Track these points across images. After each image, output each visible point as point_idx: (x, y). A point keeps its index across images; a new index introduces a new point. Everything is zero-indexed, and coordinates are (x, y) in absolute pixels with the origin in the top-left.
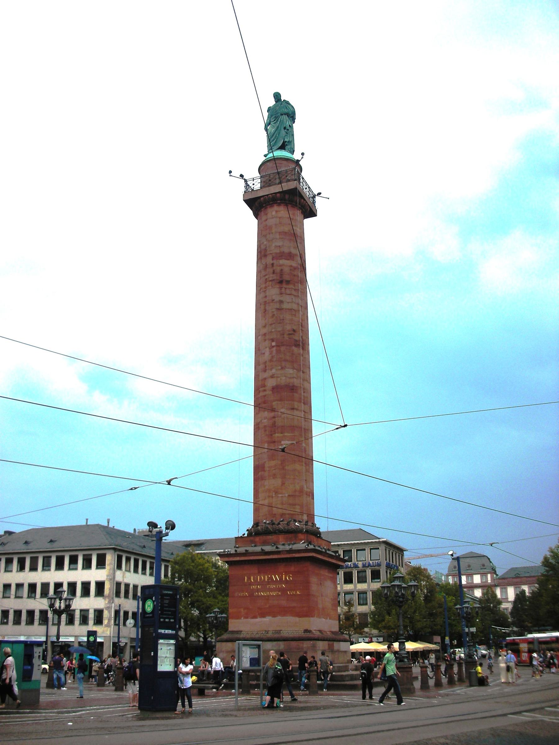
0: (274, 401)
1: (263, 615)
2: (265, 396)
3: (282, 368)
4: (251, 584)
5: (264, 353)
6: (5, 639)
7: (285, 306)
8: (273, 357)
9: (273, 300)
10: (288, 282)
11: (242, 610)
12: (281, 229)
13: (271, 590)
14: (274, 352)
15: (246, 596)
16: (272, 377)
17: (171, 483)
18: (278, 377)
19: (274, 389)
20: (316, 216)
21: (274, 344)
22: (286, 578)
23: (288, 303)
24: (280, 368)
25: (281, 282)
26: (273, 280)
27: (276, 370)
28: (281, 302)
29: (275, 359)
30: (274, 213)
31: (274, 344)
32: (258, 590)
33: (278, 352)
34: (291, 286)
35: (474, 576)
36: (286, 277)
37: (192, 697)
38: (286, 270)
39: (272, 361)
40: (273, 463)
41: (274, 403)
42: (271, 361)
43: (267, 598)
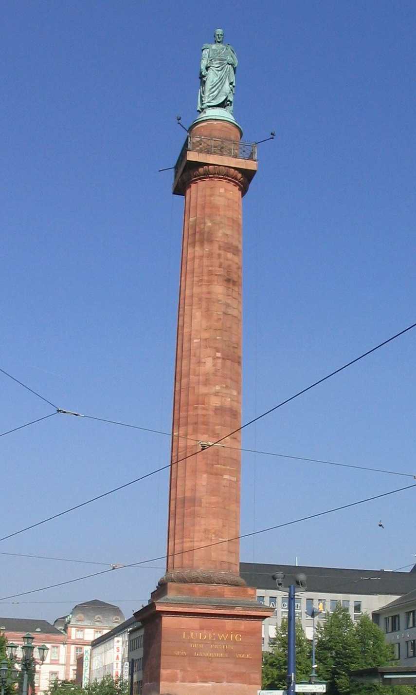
1: (205, 680)
3: (227, 387)
6: (264, 590)
7: (230, 311)
8: (216, 371)
9: (219, 301)
10: (234, 283)
11: (178, 671)
12: (230, 214)
14: (219, 366)
16: (216, 394)
19: (216, 410)
20: (174, 193)
21: (218, 355)
22: (234, 638)
23: (234, 308)
24: (224, 386)
25: (228, 280)
26: (220, 275)
27: (222, 387)
29: (219, 374)
30: (222, 190)
31: (218, 355)
32: (198, 650)
33: (223, 366)
34: (236, 289)
36: (234, 277)
38: (234, 267)
39: (216, 376)
40: (214, 499)
41: (217, 427)
42: (215, 374)
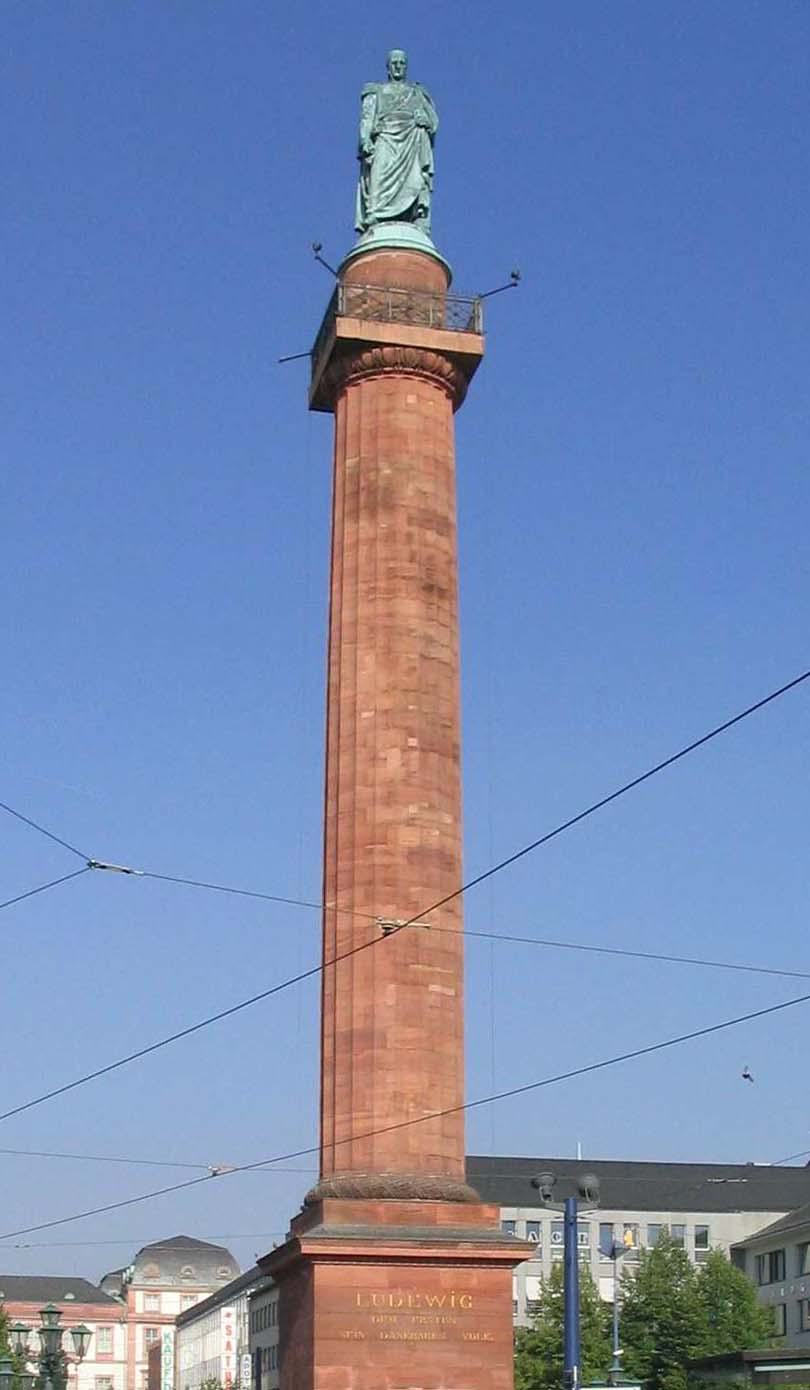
0: (414, 883)
2: (388, 866)
3: (431, 807)
4: (371, 1311)
5: (386, 759)
8: (409, 774)
12: (429, 448)
13: (419, 1327)
14: (414, 765)
15: (360, 1339)
16: (410, 822)
17: (360, 399)
18: (422, 827)
21: (413, 742)
22: (457, 1302)
23: (442, 646)
24: (426, 805)
25: (429, 588)
27: (422, 808)
28: (429, 640)
29: (414, 781)
30: (411, 399)
31: (413, 742)
33: (423, 763)
35: (163, 1293)
37: (126, 1366)
38: (441, 560)
42: (406, 782)
43: (411, 1346)
